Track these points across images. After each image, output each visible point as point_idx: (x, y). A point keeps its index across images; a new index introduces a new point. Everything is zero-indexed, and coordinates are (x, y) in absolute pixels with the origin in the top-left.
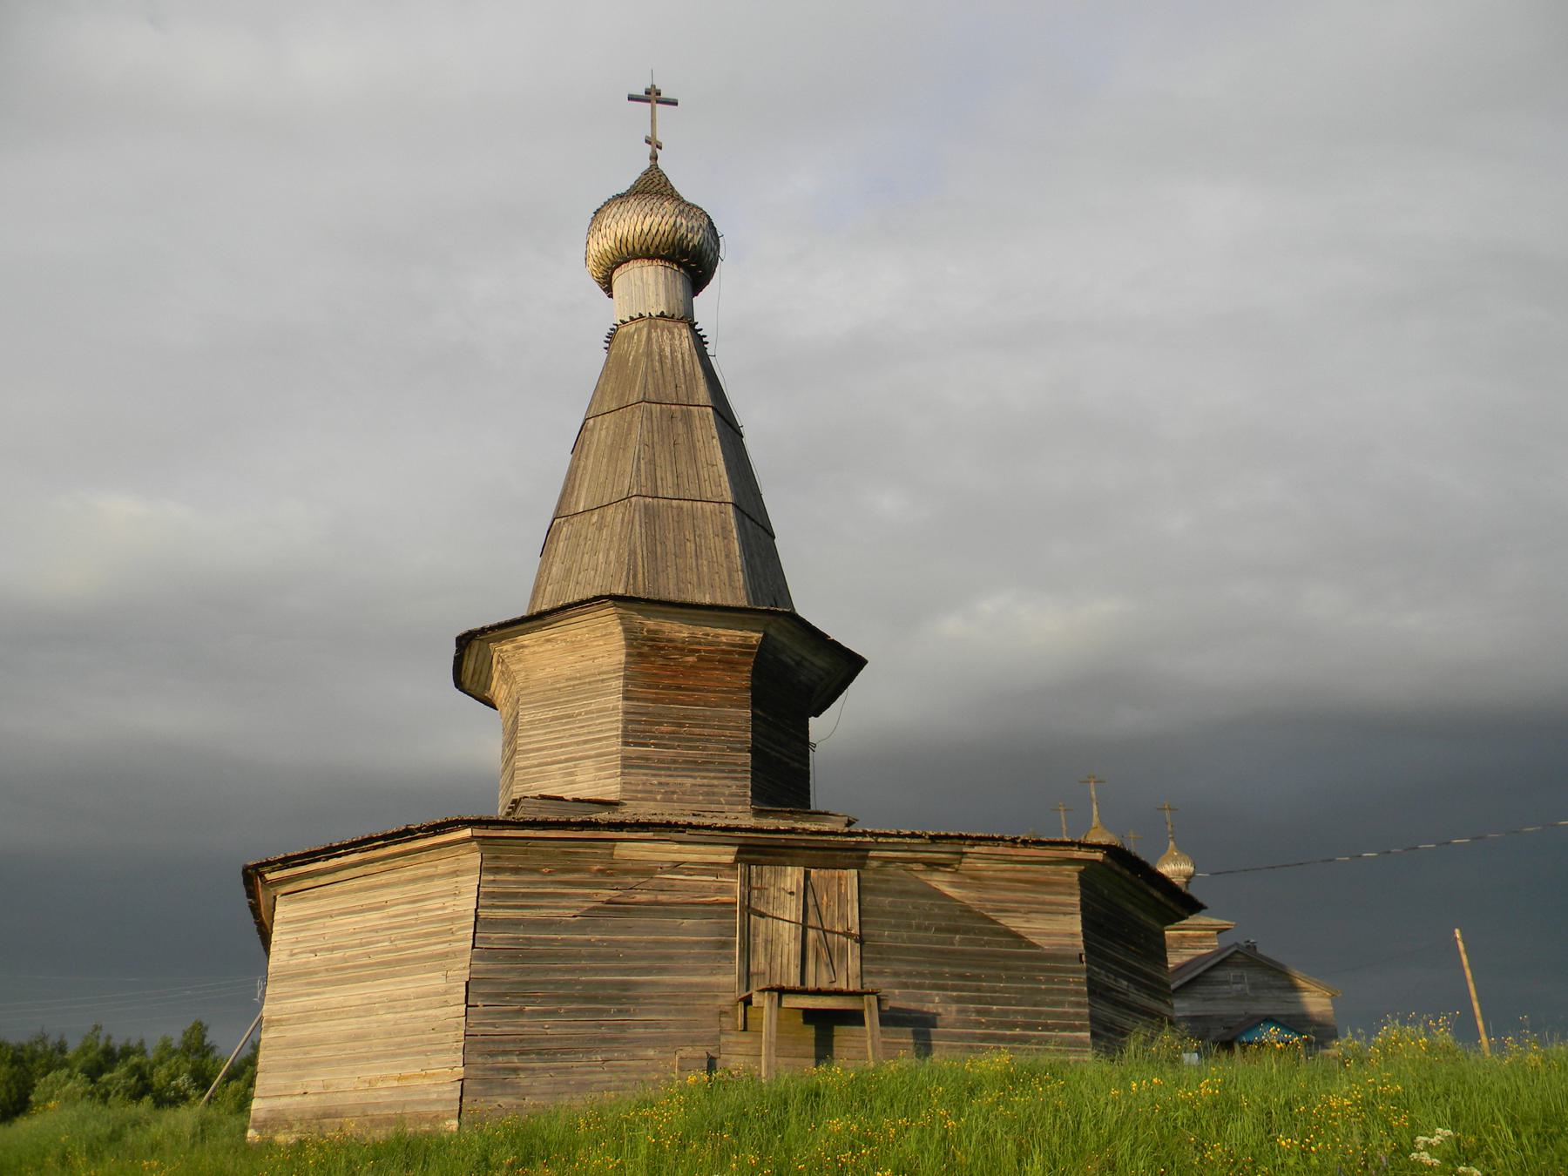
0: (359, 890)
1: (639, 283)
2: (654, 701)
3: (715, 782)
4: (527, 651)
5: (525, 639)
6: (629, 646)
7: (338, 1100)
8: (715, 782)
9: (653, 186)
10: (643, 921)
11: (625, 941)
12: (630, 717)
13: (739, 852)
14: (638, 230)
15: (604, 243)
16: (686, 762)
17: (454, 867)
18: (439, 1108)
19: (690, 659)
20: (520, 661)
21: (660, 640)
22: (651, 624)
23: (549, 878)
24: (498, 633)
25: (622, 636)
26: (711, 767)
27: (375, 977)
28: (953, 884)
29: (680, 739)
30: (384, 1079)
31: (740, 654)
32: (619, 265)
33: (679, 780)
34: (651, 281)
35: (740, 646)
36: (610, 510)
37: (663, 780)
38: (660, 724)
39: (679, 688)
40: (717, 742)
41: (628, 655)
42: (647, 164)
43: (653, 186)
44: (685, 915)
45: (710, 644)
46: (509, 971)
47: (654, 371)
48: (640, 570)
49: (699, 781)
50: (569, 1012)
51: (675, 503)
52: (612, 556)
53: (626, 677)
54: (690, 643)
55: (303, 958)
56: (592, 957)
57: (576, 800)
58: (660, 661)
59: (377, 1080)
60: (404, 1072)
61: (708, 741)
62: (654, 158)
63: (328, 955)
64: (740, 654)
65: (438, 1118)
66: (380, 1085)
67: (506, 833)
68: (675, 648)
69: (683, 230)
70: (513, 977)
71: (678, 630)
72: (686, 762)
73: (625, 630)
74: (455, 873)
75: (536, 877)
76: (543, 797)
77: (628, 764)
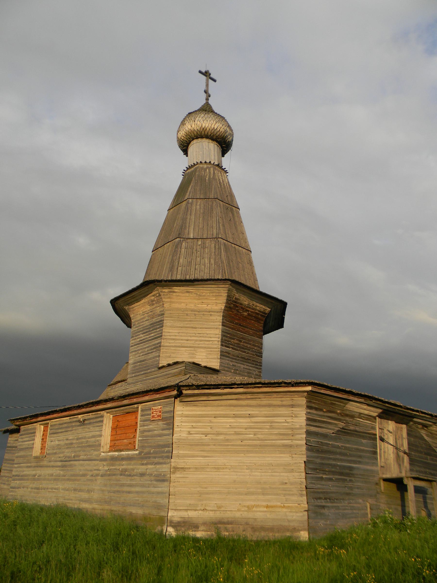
0: (230, 406)
1: (207, 148)
2: (232, 328)
3: (251, 368)
4: (174, 294)
5: (176, 289)
6: (227, 303)
7: (228, 515)
8: (251, 368)
9: (207, 109)
10: (353, 438)
11: (349, 448)
12: (224, 334)
13: (381, 413)
14: (212, 127)
15: (190, 126)
16: (242, 357)
17: (290, 403)
18: (295, 524)
19: (246, 314)
20: (170, 298)
21: (238, 303)
22: (237, 295)
23: (326, 414)
24: (168, 283)
25: (226, 298)
26: (249, 361)
27: (249, 452)
28: (427, 435)
29: (240, 347)
30: (257, 506)
31: (261, 315)
32: (197, 138)
33: (239, 365)
34: (212, 149)
35: (262, 312)
36: (208, 241)
37: (234, 364)
38: (234, 339)
39: (240, 325)
40: (252, 351)
41: (226, 307)
42: (204, 102)
43: (207, 109)
44: (364, 438)
45: (253, 309)
46: (317, 457)
47: (219, 188)
48: (226, 270)
49: (245, 367)
50: (337, 479)
51: (233, 245)
52: (212, 261)
53: (223, 316)
54: (247, 307)
55: (198, 436)
56: (341, 454)
57: (205, 367)
58: (235, 312)
59: (253, 507)
60: (269, 504)
61: (249, 350)
62: (207, 99)
63: (214, 437)
64: (261, 315)
65: (295, 530)
66: (254, 509)
67: (322, 391)
68: (242, 308)
69: (228, 134)
70: (318, 461)
71: (245, 300)
72: (242, 357)
73: (228, 296)
74: (292, 406)
75: (321, 413)
76: (194, 363)
77: (223, 354)
